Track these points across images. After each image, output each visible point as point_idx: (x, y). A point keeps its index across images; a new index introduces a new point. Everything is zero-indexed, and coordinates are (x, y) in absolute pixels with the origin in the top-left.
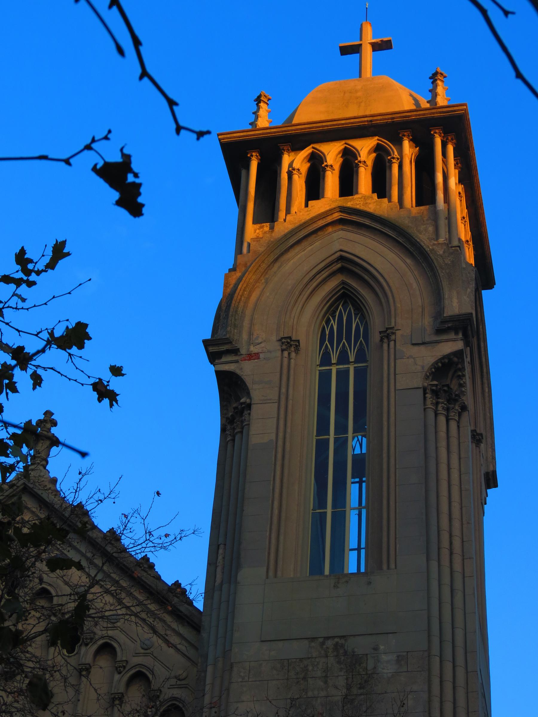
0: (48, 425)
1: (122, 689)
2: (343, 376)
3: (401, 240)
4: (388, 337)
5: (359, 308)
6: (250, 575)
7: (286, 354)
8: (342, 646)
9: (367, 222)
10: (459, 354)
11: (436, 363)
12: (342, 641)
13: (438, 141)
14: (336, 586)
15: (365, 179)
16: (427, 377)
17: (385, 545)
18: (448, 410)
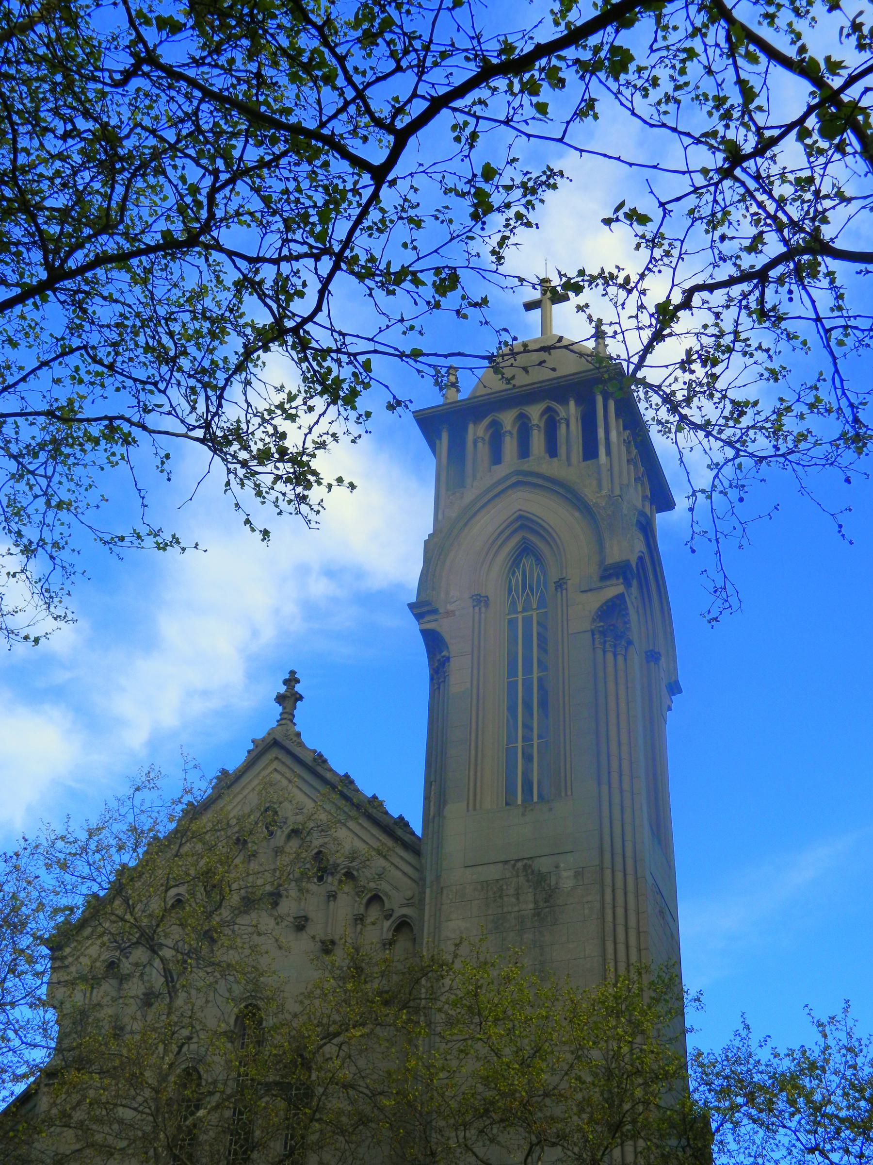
0: (293, 683)
1: (362, 910)
2: (527, 621)
3: (569, 496)
4: (561, 586)
5: (539, 560)
6: (454, 810)
7: (477, 609)
8: (530, 866)
9: (540, 482)
10: (621, 597)
11: (602, 606)
12: (530, 862)
13: (600, 400)
14: (523, 815)
15: (538, 440)
16: (594, 620)
17: (563, 774)
18: (615, 646)
